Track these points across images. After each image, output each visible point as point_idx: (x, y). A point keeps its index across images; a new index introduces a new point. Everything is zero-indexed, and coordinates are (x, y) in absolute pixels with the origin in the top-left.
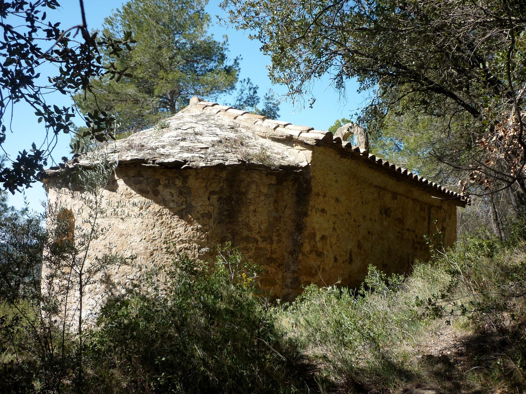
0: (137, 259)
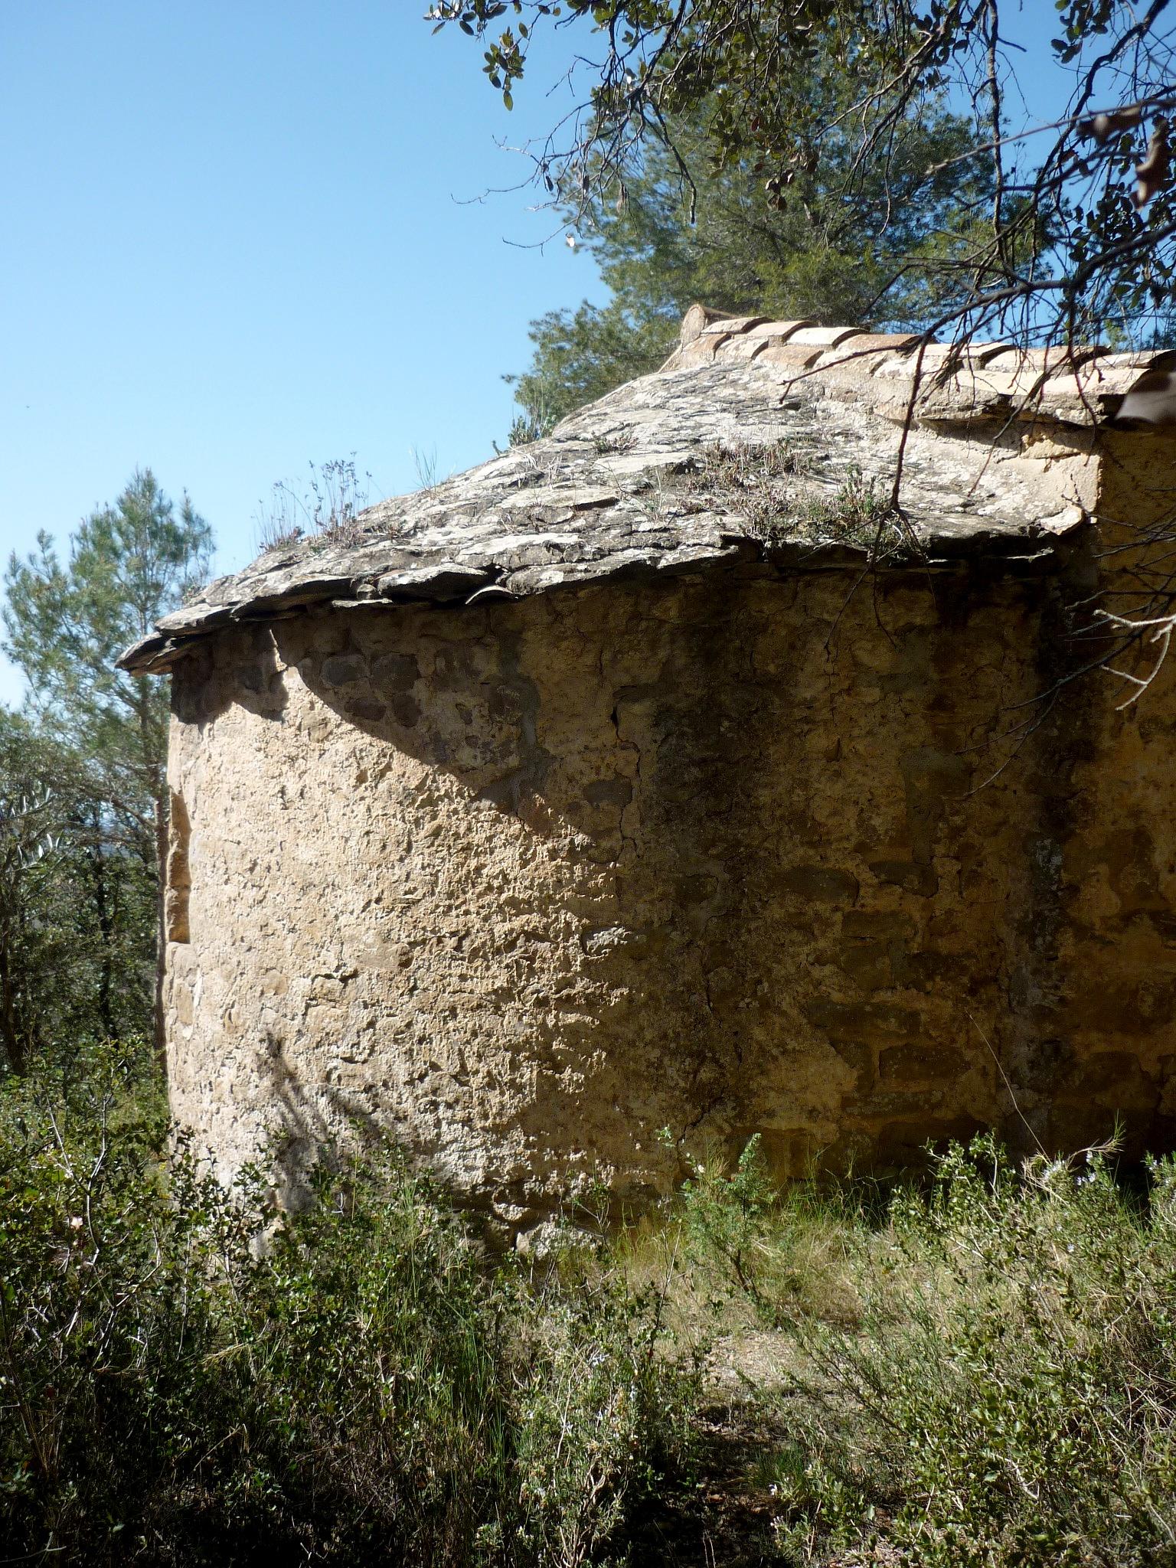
0: (359, 979)
